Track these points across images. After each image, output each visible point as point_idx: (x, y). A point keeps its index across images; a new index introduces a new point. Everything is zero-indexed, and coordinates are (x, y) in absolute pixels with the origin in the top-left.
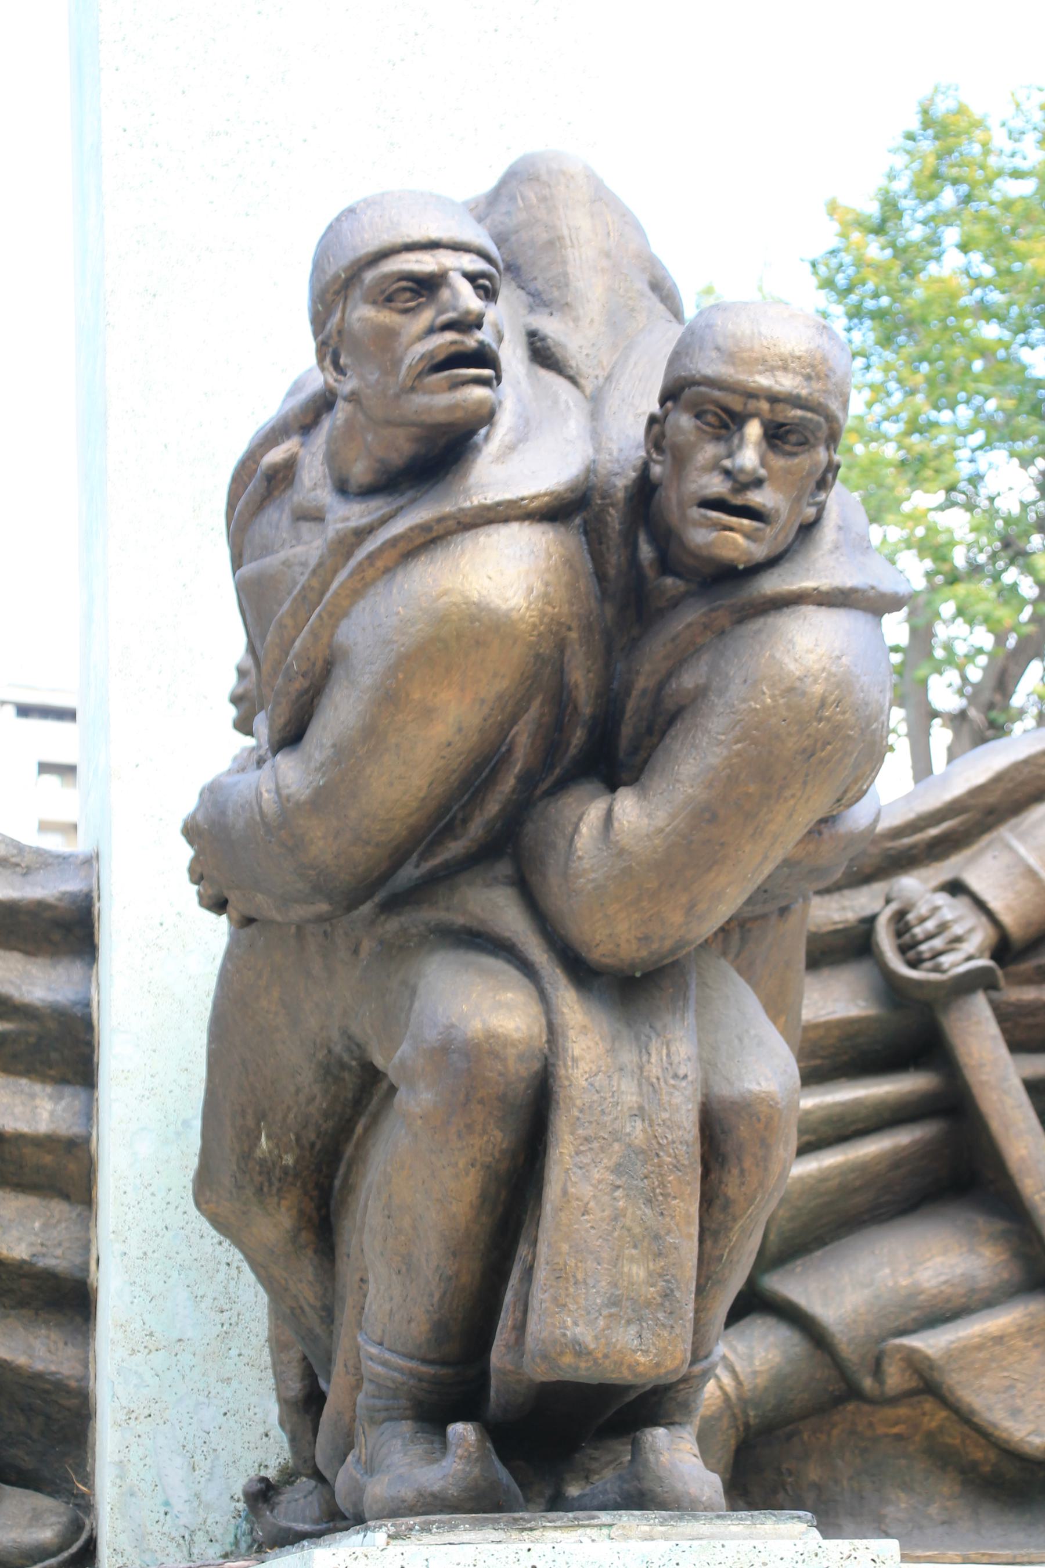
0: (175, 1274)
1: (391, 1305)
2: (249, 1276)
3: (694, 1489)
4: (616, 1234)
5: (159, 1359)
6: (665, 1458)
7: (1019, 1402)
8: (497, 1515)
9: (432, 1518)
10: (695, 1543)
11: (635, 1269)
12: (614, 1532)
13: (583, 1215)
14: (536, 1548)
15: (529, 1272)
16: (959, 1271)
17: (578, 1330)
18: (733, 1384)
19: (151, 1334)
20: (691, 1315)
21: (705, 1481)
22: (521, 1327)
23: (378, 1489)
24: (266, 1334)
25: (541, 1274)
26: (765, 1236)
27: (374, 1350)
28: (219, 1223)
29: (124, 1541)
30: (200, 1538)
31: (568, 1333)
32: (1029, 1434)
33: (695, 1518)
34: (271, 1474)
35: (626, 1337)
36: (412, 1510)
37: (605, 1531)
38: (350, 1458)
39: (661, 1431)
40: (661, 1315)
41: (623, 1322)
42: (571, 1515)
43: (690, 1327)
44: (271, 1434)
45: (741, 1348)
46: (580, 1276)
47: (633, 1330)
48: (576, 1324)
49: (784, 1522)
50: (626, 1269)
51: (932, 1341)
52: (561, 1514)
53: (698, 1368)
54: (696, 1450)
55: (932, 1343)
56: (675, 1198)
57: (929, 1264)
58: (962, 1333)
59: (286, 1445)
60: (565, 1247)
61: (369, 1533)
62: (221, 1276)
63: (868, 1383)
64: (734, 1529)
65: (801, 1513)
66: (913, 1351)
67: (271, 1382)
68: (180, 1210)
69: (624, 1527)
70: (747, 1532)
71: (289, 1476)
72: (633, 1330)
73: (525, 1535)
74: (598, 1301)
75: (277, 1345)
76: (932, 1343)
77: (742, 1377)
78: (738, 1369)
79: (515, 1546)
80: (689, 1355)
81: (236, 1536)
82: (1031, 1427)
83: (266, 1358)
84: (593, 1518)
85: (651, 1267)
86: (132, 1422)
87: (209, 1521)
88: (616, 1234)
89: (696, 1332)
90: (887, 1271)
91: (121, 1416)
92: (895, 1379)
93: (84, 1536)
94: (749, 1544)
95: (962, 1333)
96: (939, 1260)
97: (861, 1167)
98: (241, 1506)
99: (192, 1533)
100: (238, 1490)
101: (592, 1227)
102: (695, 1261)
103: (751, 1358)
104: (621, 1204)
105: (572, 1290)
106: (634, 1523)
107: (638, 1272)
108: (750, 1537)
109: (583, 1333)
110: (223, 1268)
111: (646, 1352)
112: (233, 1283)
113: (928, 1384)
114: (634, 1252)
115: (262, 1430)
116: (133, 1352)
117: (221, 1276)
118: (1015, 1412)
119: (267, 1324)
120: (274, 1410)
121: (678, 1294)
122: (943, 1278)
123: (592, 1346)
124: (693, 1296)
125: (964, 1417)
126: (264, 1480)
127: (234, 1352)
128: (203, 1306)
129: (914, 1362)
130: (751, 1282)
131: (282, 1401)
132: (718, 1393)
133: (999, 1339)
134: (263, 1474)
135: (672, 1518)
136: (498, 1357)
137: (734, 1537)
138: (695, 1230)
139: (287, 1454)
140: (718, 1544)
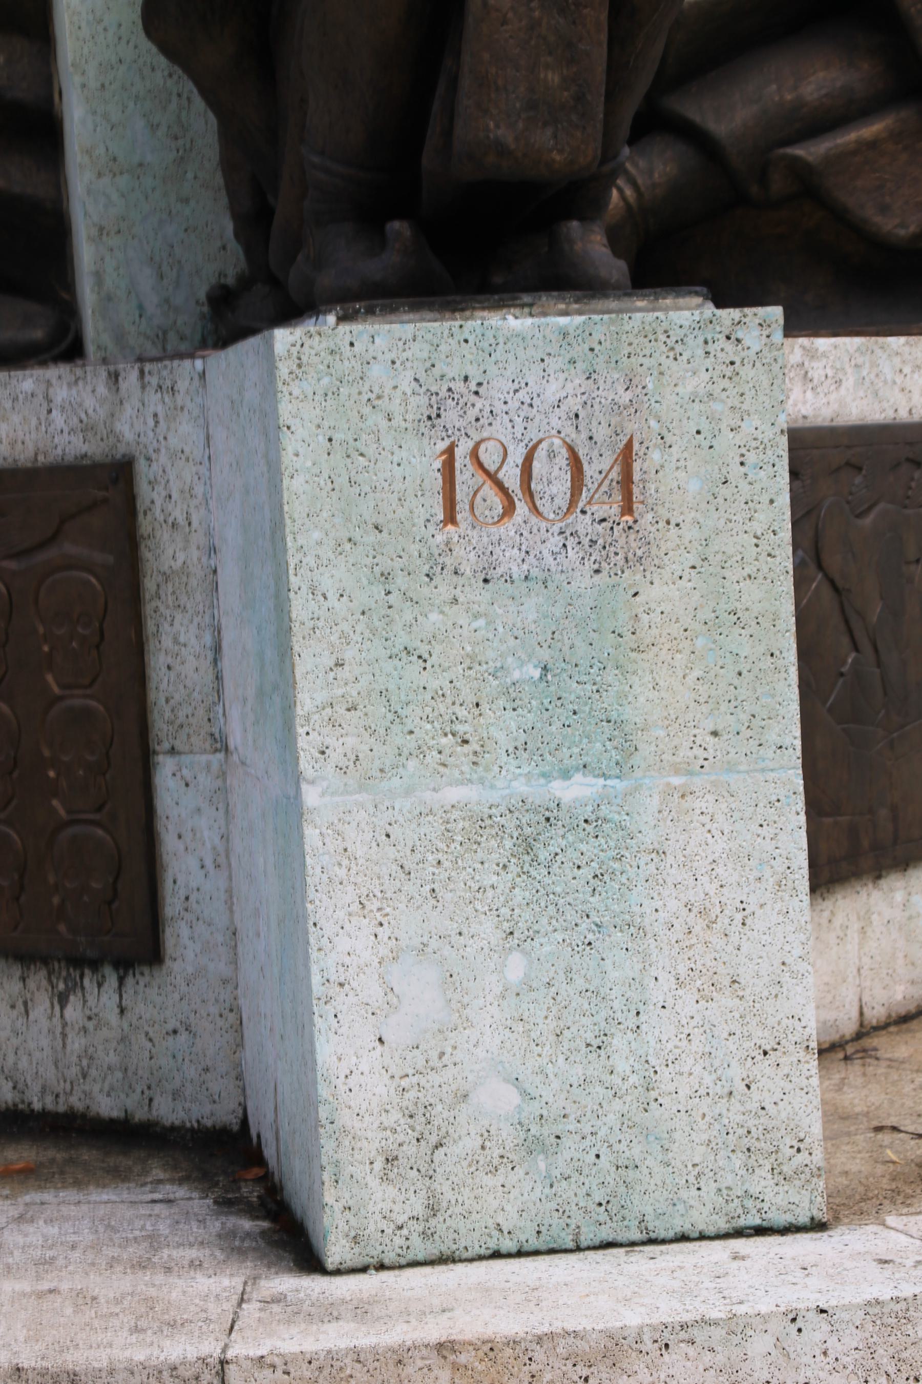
0: (131, 105)
1: (329, 116)
2: (199, 103)
3: (603, 273)
4: (533, 43)
5: (123, 181)
6: (578, 246)
7: (888, 199)
8: (432, 299)
9: (375, 302)
10: (606, 317)
11: (550, 75)
12: (535, 310)
13: (502, 25)
14: (470, 324)
15: (454, 82)
16: (839, 84)
17: (500, 132)
18: (635, 195)
19: (115, 159)
20: (601, 116)
21: (616, 268)
22: (448, 133)
23: (326, 280)
24: (218, 158)
25: (466, 83)
26: (663, 60)
27: (316, 159)
28: (166, 49)
29: (106, 339)
30: (172, 336)
31: (492, 136)
32: (896, 227)
33: (606, 296)
34: (230, 281)
35: (543, 138)
36: (357, 297)
37: (526, 310)
38: (300, 257)
39: (575, 224)
40: (574, 117)
41: (540, 124)
42: (496, 297)
43: (600, 126)
44: (229, 247)
45: (642, 163)
46: (500, 82)
47: (549, 132)
48: (497, 126)
49: (683, 296)
50: (542, 76)
51: (812, 149)
52: (488, 296)
53: (607, 168)
54: (605, 241)
55: (812, 152)
56: (586, 7)
57: (812, 79)
58: (840, 141)
59: (242, 256)
60: (486, 56)
61: (321, 317)
62: (173, 106)
63: (754, 189)
64: (640, 304)
65: (698, 289)
66: (796, 159)
67: (224, 200)
68: (131, 44)
69: (543, 306)
70: (651, 306)
71: (245, 283)
72: (549, 132)
73: (457, 315)
74: (518, 105)
75: (228, 166)
76: (812, 152)
77: (643, 189)
78: (640, 181)
79: (449, 323)
80: (599, 152)
81: (203, 335)
82: (897, 221)
83: (219, 180)
84: (516, 298)
85: (565, 72)
86: (104, 238)
87: (179, 322)
88: (533, 43)
89: (605, 135)
90: (774, 87)
91: (94, 232)
92: (778, 184)
93: (71, 337)
94: (651, 316)
95: (840, 141)
96: (821, 75)
98: (206, 309)
99: (165, 333)
100: (202, 294)
101: (511, 37)
102: (605, 66)
103: (647, 173)
104: (537, 14)
105: (493, 96)
106: (552, 303)
107: (553, 78)
108: (654, 310)
109: (504, 134)
110: (175, 99)
111: (561, 151)
112: (184, 114)
113: (808, 185)
114: (549, 59)
115: (219, 244)
116: (100, 175)
117: (173, 106)
118: (884, 209)
119: (218, 150)
120: (229, 227)
121: (589, 98)
122: (823, 92)
123: (513, 146)
124: (603, 98)
125: (840, 217)
126: (224, 287)
127: (190, 175)
128: (159, 133)
129: (798, 168)
130: (650, 99)
131: (236, 217)
132: (622, 204)
133: (872, 145)
134: (222, 281)
135: (585, 297)
136: (428, 160)
137: (640, 310)
138: (604, 37)
139: (243, 264)
140: (626, 317)
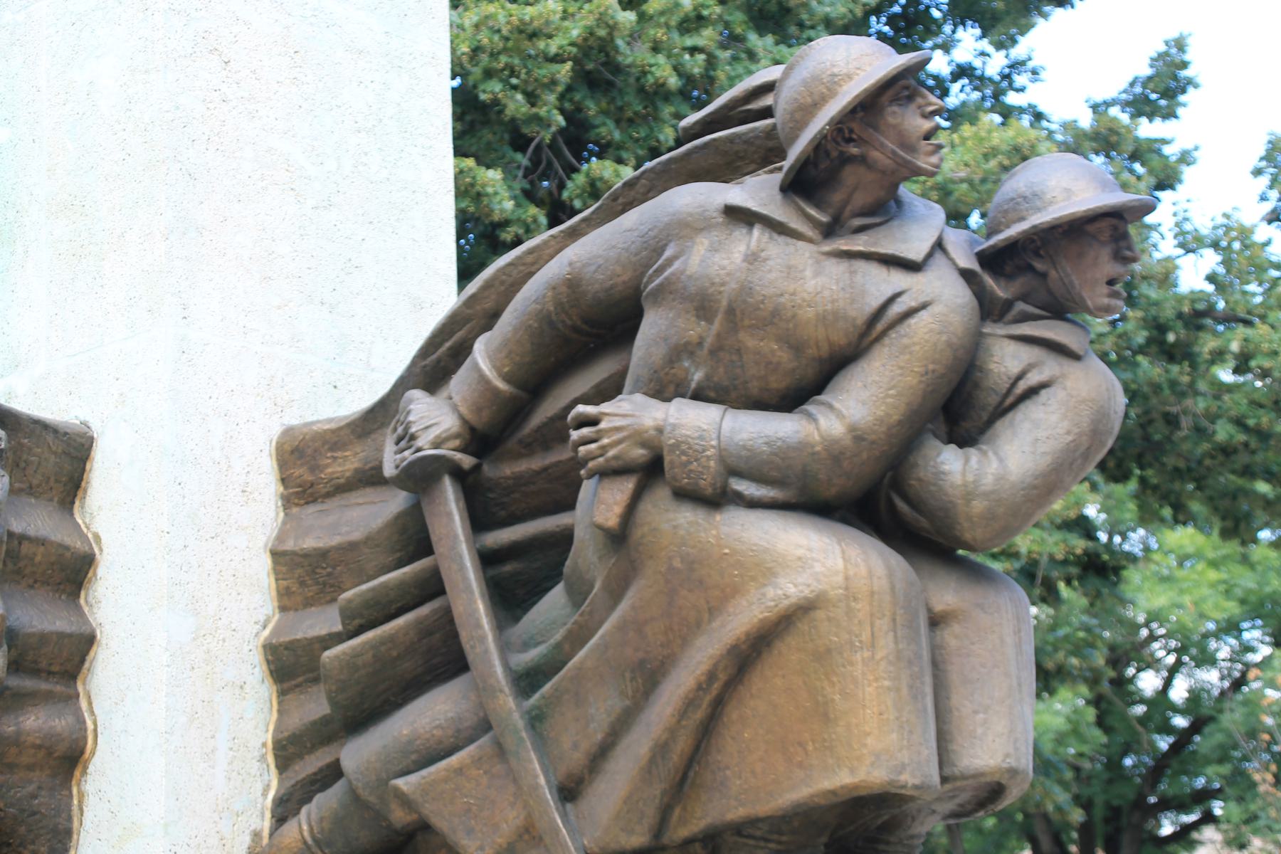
97: (391, 639)
133: (460, 771)
